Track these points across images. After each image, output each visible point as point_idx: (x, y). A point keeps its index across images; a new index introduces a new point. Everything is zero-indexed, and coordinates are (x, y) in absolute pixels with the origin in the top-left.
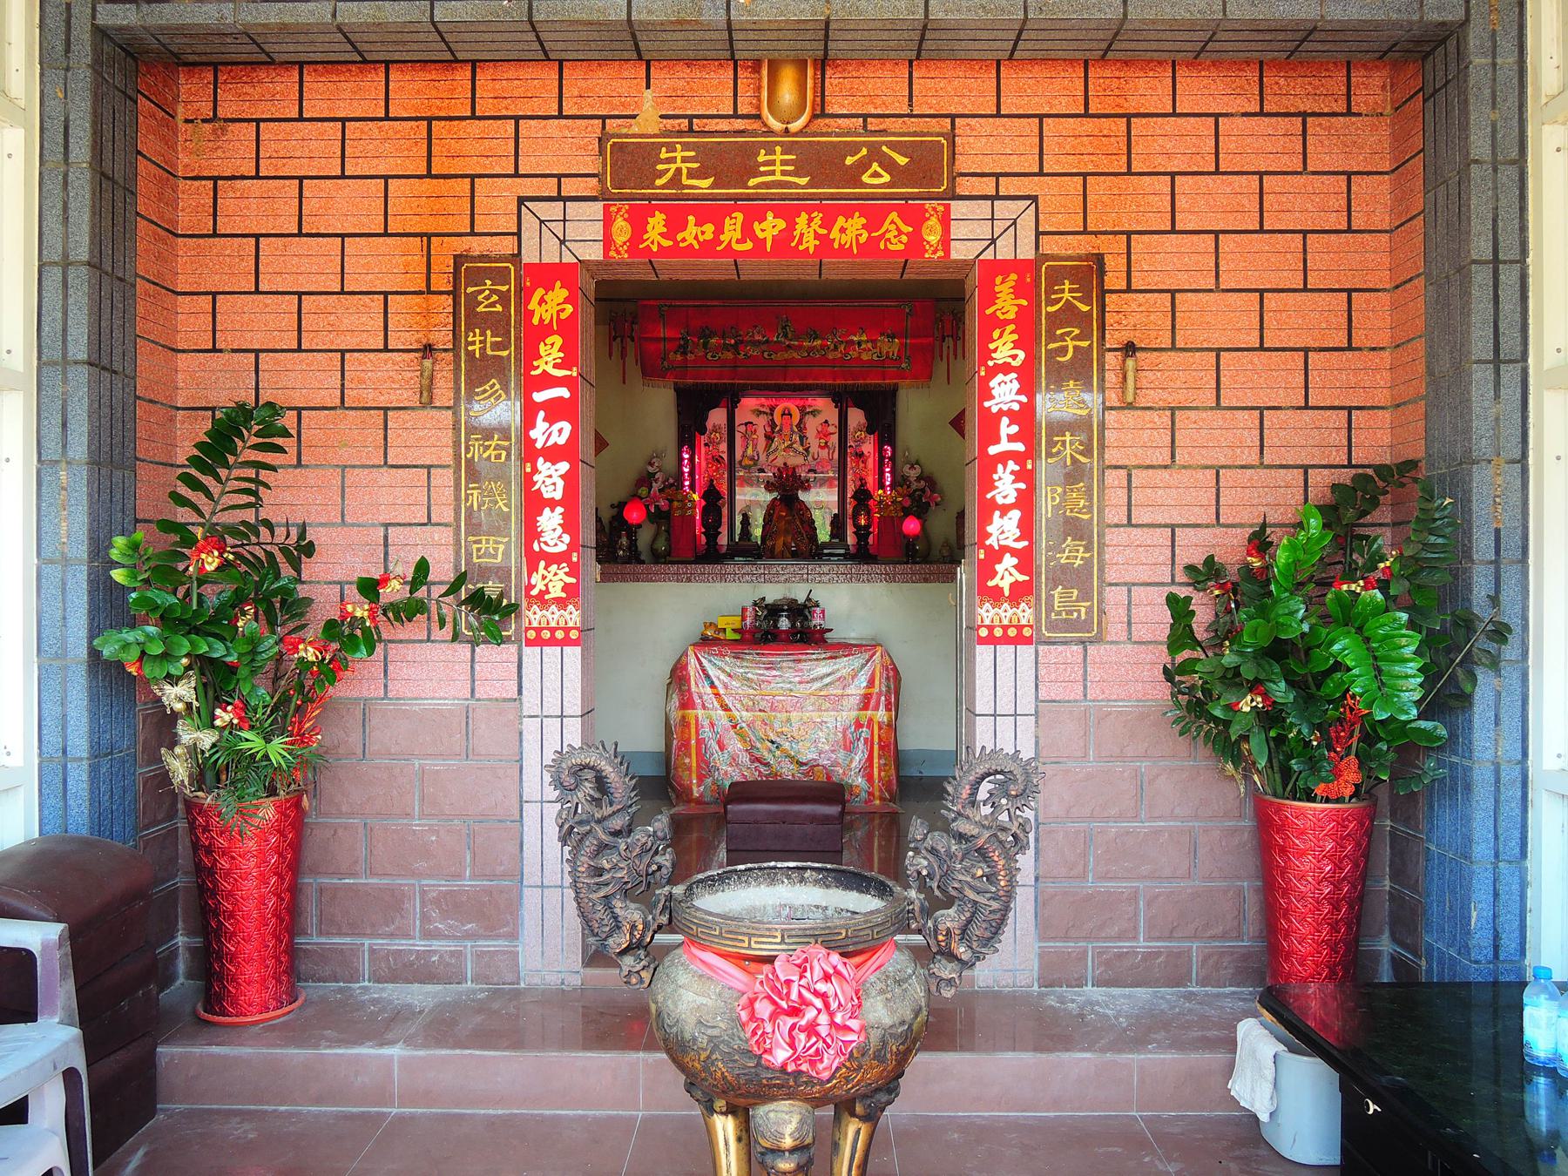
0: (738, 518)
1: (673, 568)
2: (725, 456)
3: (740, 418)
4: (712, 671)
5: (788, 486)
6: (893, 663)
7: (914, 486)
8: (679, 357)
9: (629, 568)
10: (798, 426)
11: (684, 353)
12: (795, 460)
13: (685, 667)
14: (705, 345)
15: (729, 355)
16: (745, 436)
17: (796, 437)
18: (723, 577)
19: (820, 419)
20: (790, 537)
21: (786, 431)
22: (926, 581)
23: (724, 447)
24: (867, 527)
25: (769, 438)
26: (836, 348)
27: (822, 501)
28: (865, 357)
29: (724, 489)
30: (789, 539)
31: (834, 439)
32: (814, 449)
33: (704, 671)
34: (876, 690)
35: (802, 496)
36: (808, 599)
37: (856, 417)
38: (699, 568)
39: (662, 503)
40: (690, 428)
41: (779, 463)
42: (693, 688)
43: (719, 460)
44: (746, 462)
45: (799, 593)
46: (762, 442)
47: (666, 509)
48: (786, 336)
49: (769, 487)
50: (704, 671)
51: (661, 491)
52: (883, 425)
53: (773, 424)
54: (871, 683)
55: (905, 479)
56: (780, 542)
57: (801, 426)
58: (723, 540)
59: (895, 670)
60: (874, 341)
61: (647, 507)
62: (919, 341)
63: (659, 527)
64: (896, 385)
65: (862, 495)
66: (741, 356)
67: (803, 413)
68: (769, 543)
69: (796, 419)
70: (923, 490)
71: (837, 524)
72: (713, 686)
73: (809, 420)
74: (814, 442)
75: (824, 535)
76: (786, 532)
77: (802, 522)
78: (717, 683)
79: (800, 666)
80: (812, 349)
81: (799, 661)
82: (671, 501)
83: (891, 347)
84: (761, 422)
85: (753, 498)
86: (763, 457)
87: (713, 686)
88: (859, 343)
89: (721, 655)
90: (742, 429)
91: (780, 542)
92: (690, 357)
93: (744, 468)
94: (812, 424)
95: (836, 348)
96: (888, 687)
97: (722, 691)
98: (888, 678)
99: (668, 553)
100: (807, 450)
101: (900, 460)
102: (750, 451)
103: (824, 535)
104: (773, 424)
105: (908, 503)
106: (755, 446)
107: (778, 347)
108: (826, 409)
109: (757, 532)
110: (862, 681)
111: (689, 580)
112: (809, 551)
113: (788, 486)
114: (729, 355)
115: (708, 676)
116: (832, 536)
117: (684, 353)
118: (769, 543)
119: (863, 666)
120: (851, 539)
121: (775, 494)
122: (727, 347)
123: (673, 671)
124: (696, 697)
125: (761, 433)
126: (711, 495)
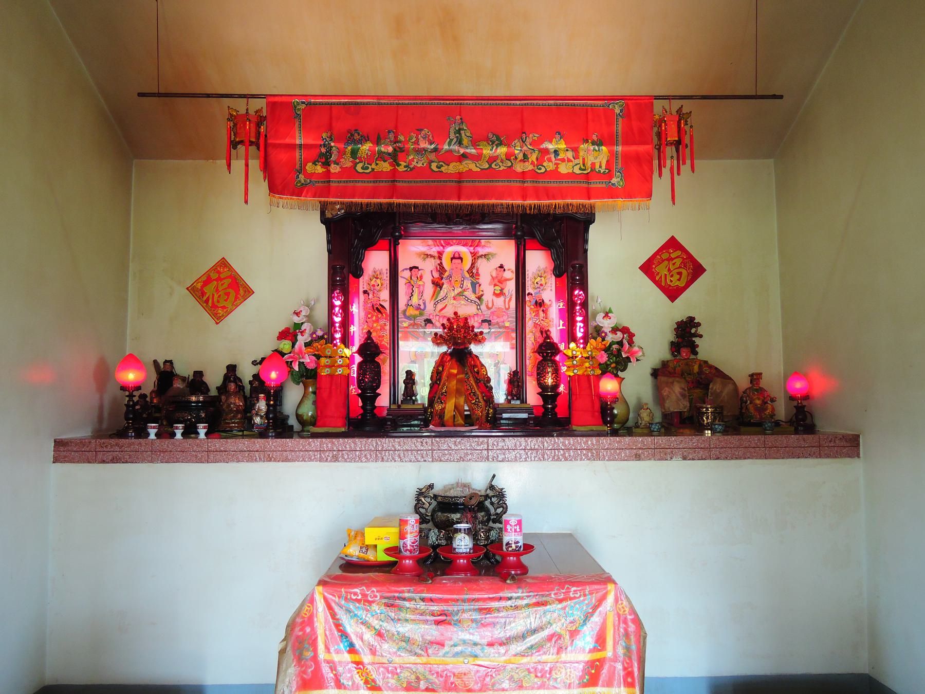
0: (402, 377)
1: (316, 443)
2: (387, 305)
3: (404, 263)
4: (350, 627)
5: (458, 342)
6: (633, 611)
7: (610, 338)
8: (319, 169)
9: (272, 443)
10: (470, 271)
11: (326, 164)
12: (466, 309)
13: (310, 621)
14: (354, 153)
15: (385, 167)
16: (410, 284)
17: (467, 284)
18: (378, 455)
19: (495, 263)
20: (461, 405)
21: (456, 277)
22: (638, 457)
23: (385, 295)
24: (555, 387)
25: (438, 284)
26: (525, 158)
27: (496, 356)
28: (564, 169)
29: (386, 341)
30: (462, 400)
31: (511, 287)
32: (488, 296)
33: (338, 626)
34: (609, 653)
35: (474, 348)
36: (517, 553)
37: (537, 260)
38: (349, 443)
39: (307, 360)
40: (343, 270)
41: (449, 312)
42: (322, 655)
43: (379, 309)
44: (411, 311)
45: (476, 475)
46: (429, 289)
47: (312, 366)
48: (460, 143)
49: (438, 340)
50: (338, 626)
51: (307, 345)
52: (572, 270)
53: (441, 269)
54: (600, 640)
55: (598, 330)
56: (450, 406)
57: (473, 273)
58: (384, 401)
59: (637, 622)
60: (576, 150)
61: (289, 364)
62: (633, 148)
63: (306, 388)
64: (592, 207)
65: (547, 350)
66: (401, 169)
67: (475, 256)
68: (438, 407)
69: (467, 264)
70: (620, 343)
71: (516, 383)
72: (352, 650)
73: (482, 264)
74: (487, 289)
75: (500, 395)
76: (458, 392)
77: (477, 381)
78: (358, 644)
79: (489, 618)
80: (492, 159)
81: (489, 611)
82: (318, 357)
83: (596, 156)
84: (428, 268)
85: (419, 356)
86: (430, 307)
87: (352, 650)
88: (556, 152)
89: (366, 601)
90: (407, 274)
91: (450, 406)
92: (334, 169)
93: (408, 318)
94: (486, 269)
95: (525, 158)
96: (628, 649)
97: (367, 658)
98: (627, 635)
99: (314, 422)
100: (479, 298)
101: (592, 307)
102: (415, 300)
103: (500, 395)
104: (441, 269)
105: (604, 358)
106: (421, 294)
107: (449, 157)
108: (502, 252)
109: (423, 392)
110: (586, 640)
111: (335, 459)
112: (490, 420)
113: (458, 342)
114: (385, 167)
115: (344, 634)
116: (509, 393)
117: (326, 164)
118: (438, 407)
119: (587, 617)
120: (532, 397)
121: (444, 349)
122: (382, 157)
123: (291, 627)
124: (325, 669)
125: (427, 279)
126: (370, 350)
